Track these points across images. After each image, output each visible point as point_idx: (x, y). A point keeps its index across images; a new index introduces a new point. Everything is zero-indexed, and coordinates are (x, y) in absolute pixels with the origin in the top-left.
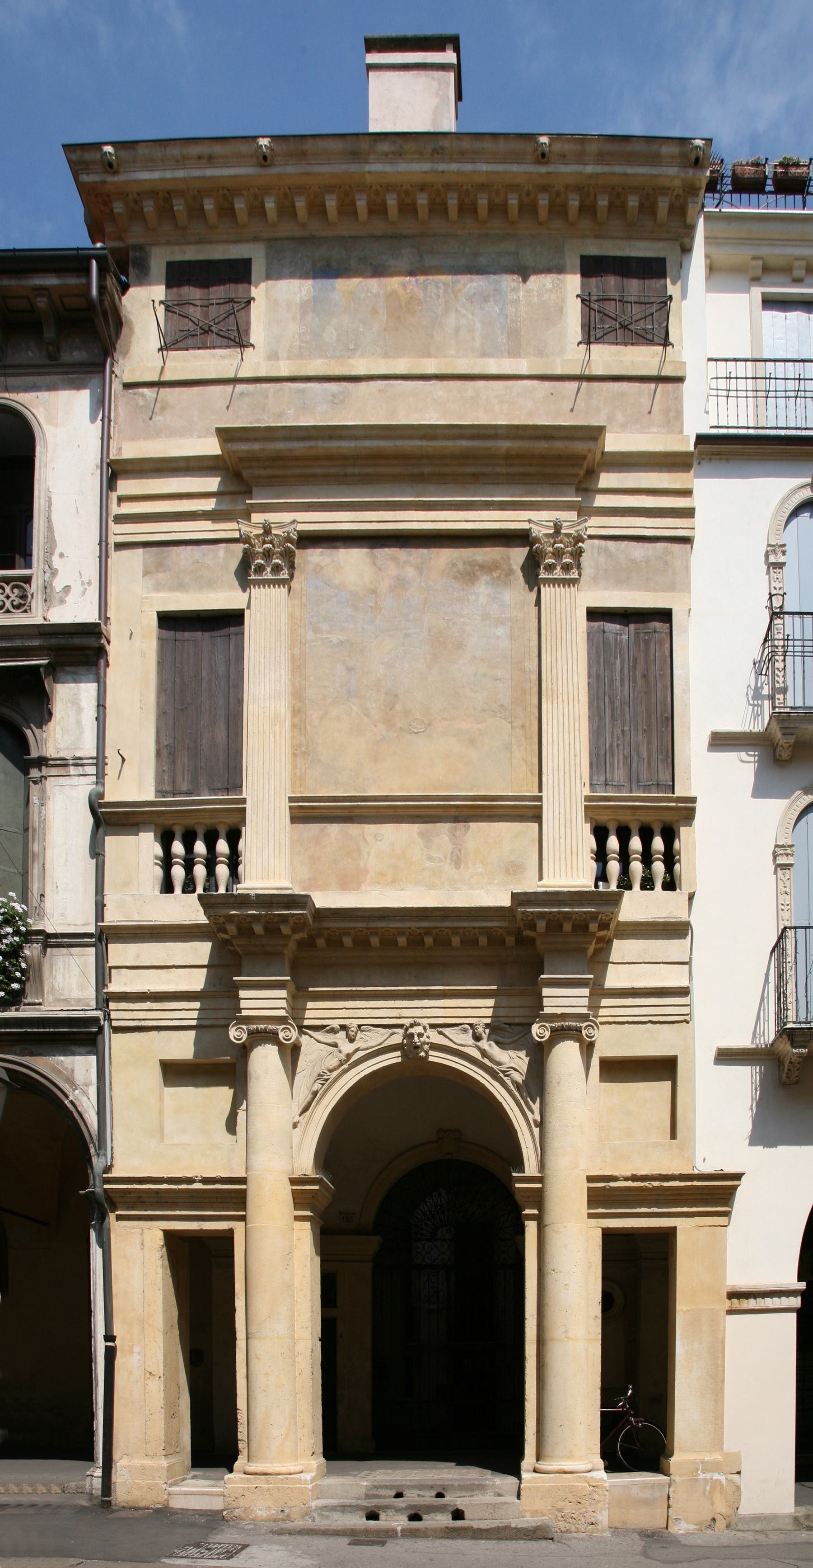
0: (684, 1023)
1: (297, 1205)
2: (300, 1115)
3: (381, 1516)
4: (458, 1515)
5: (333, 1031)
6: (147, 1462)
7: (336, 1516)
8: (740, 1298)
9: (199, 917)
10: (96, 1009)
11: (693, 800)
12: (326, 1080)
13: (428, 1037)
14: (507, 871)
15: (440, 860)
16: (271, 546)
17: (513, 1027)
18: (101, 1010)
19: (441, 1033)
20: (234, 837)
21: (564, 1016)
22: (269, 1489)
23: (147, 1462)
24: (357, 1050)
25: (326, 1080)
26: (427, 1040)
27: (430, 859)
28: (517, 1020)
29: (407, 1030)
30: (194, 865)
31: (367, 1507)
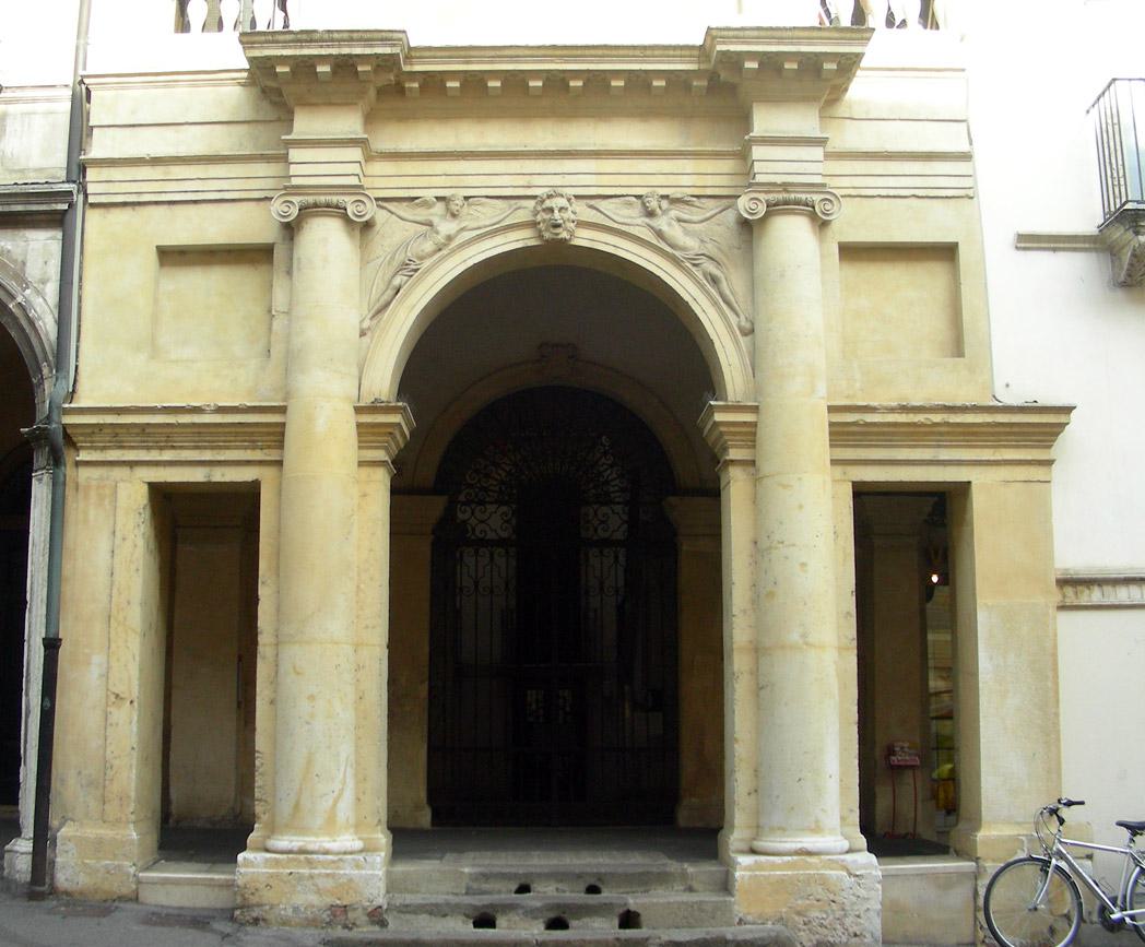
0: (966, 200)
1: (363, 443)
2: (372, 318)
3: (497, 922)
4: (629, 919)
5: (426, 204)
6: (106, 832)
7: (423, 919)
10: (68, 182)
12: (416, 270)
13: (574, 213)
18: (74, 182)
21: (785, 187)
22: (311, 877)
23: (106, 832)
24: (463, 229)
25: (416, 270)
26: (573, 217)
28: (709, 192)
29: (543, 202)
31: (475, 908)
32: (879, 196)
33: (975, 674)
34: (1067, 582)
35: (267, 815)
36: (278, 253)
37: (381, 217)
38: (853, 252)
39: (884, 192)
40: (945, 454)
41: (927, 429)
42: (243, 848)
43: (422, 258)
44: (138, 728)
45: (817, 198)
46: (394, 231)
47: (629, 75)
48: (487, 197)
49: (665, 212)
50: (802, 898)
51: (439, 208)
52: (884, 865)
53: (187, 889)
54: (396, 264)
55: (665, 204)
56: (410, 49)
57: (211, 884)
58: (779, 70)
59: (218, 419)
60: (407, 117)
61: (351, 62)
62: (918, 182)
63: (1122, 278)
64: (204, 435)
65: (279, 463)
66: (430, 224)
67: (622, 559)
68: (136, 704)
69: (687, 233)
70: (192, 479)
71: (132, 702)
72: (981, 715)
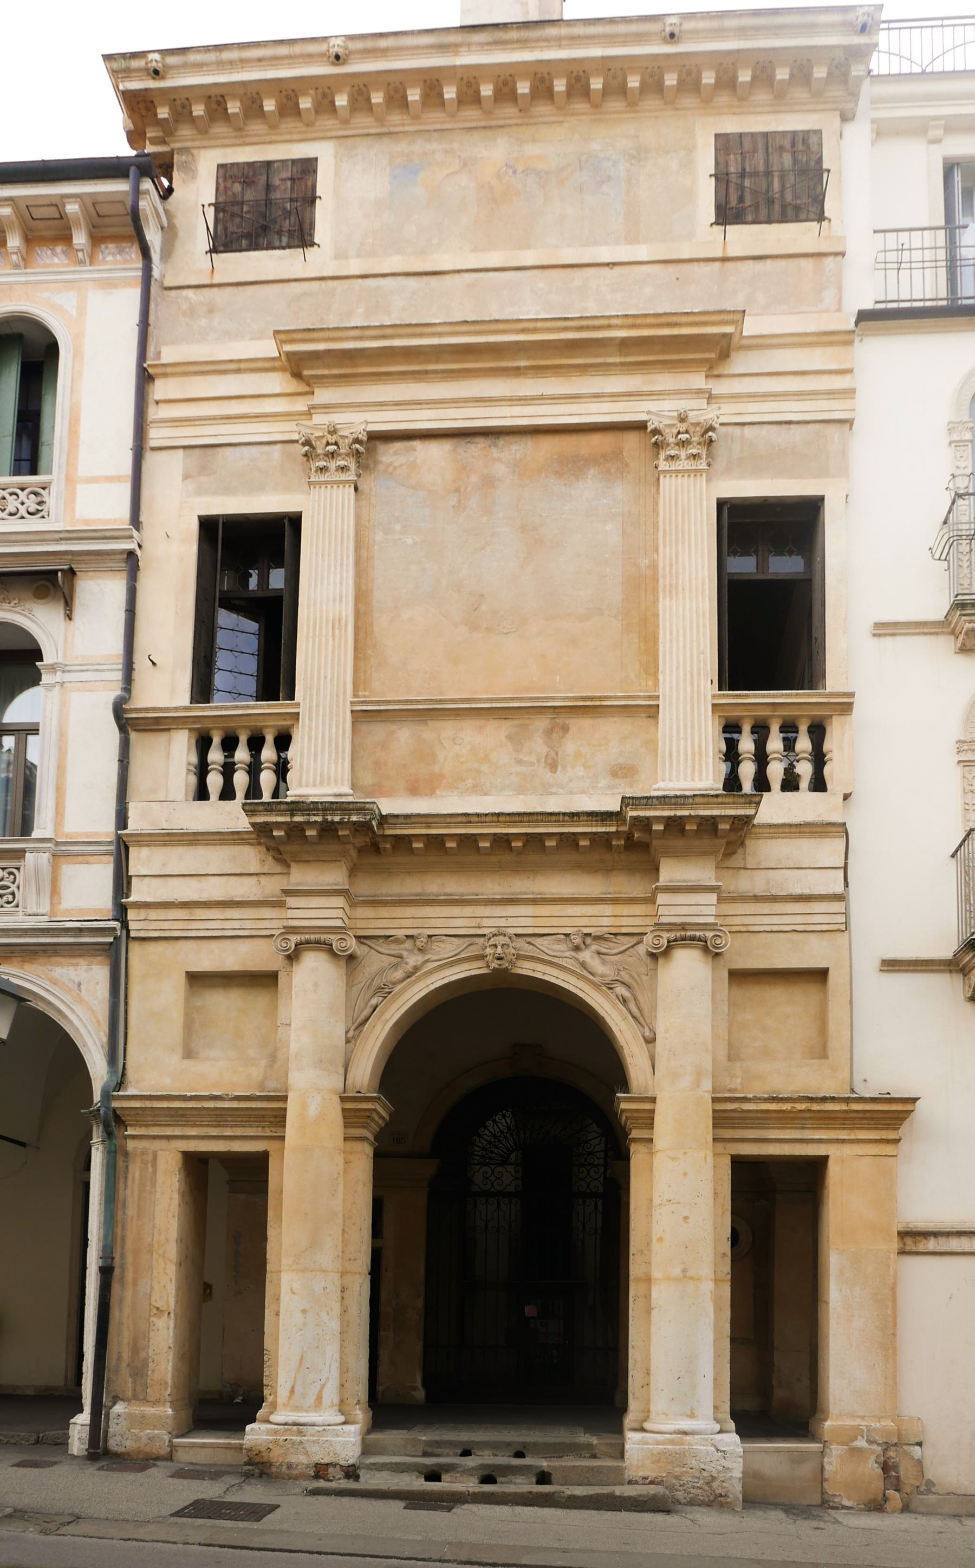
2: (355, 1030)
5: (398, 941)
9: (243, 823)
11: (852, 695)
16: (335, 447)
17: (619, 937)
19: (529, 943)
20: (283, 742)
21: (683, 927)
22: (301, 1442)
24: (427, 961)
25: (390, 993)
27: (519, 762)
28: (624, 930)
30: (234, 771)
32: (765, 931)
37: (360, 951)
38: (739, 977)
40: (808, 1134)
41: (794, 1115)
42: (253, 1420)
43: (395, 984)
44: (174, 1333)
45: (710, 934)
46: (375, 962)
48: (446, 935)
50: (678, 1466)
53: (210, 1450)
54: (373, 988)
56: (382, 817)
57: (228, 1447)
58: (682, 831)
59: (235, 1105)
60: (387, 872)
61: (333, 827)
62: (799, 919)
64: (220, 1117)
66: (401, 957)
67: (600, 1207)
68: (172, 1315)
69: (604, 962)
72: (831, 1333)
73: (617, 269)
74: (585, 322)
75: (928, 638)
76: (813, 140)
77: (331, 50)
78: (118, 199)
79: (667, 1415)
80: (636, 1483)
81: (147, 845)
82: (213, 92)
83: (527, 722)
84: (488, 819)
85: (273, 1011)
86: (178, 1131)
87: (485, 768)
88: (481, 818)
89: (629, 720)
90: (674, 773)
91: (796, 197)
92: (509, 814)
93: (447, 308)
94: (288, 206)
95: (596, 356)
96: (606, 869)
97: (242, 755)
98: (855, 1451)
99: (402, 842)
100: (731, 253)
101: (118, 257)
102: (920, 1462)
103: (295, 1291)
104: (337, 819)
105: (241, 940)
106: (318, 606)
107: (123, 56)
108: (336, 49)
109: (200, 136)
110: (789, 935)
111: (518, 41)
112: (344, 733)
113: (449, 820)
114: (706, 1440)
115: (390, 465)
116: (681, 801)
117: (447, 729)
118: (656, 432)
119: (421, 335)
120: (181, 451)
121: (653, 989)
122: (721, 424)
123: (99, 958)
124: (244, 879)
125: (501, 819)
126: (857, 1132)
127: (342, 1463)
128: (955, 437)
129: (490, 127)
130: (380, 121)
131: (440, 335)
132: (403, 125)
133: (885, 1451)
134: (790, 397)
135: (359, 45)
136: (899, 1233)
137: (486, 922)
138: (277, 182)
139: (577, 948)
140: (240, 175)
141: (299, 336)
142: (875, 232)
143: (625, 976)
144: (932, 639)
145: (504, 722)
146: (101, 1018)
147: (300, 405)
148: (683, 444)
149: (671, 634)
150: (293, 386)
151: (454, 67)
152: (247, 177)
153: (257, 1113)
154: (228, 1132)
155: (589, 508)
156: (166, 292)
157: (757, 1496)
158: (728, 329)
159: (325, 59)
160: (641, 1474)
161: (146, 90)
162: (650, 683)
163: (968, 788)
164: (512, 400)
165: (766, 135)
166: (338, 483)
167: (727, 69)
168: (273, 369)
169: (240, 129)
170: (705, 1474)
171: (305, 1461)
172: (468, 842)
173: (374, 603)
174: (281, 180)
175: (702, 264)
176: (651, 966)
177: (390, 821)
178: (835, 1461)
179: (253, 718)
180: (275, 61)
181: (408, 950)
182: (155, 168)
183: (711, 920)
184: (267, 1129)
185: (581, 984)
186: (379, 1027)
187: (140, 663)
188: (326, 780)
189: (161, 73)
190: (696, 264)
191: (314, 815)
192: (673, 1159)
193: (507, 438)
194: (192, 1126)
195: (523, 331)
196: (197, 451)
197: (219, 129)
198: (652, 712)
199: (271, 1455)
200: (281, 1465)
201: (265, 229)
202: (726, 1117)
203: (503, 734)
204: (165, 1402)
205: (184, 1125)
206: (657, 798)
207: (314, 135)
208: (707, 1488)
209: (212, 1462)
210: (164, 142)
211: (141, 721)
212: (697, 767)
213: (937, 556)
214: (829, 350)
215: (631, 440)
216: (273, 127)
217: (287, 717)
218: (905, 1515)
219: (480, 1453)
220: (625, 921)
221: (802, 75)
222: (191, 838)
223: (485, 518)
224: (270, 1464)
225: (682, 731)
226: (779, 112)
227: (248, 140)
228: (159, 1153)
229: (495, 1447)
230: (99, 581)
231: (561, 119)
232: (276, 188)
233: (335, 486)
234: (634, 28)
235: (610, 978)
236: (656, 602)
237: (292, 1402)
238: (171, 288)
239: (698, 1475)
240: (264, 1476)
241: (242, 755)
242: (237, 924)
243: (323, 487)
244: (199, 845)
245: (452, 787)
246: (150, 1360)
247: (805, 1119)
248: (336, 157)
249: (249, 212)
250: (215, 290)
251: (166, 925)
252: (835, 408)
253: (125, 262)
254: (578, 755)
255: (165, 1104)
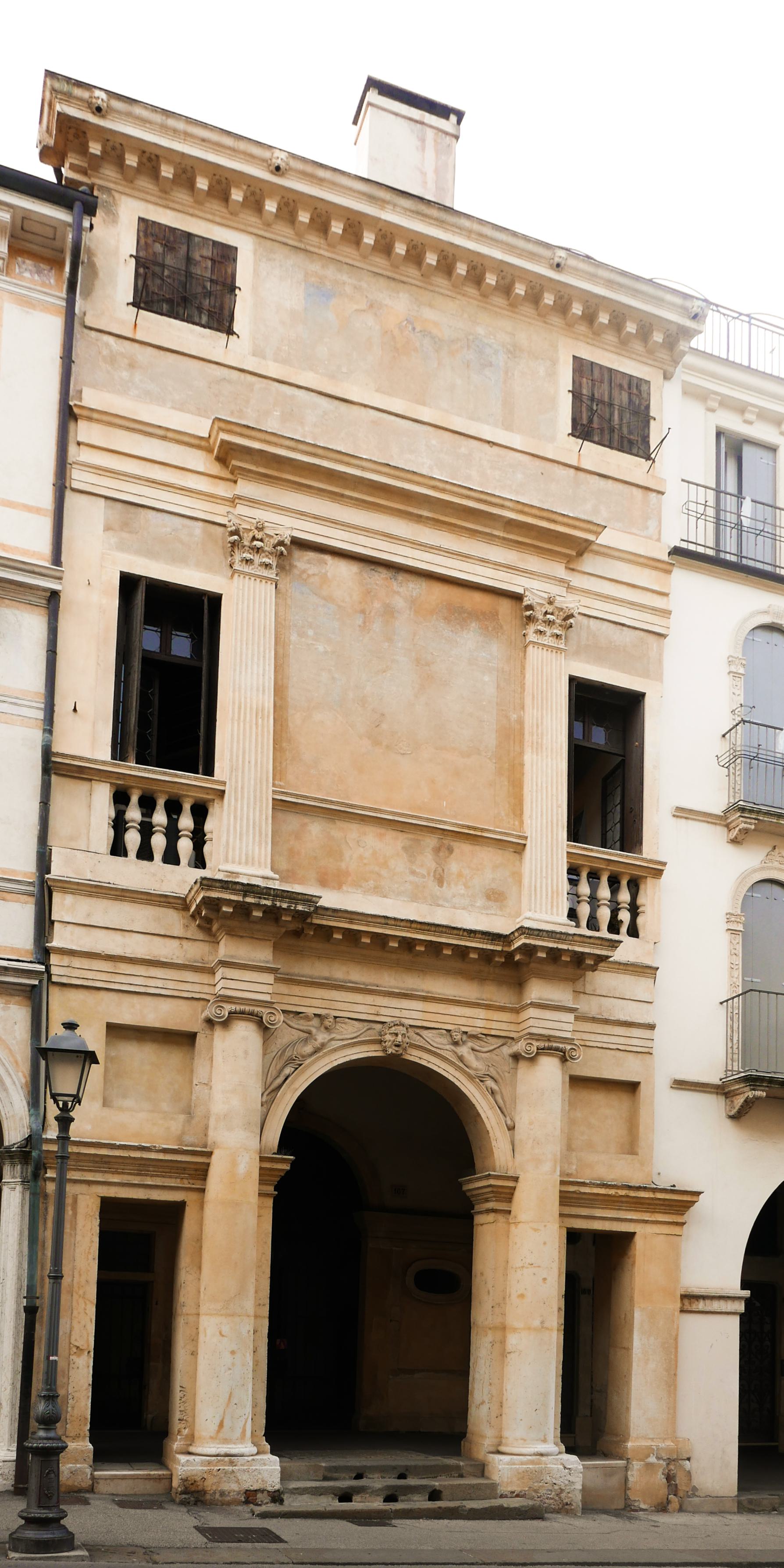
1: (262, 1182)
5: (307, 1018)
8: (691, 1301)
11: (664, 864)
14: (488, 897)
15: (423, 876)
19: (417, 1034)
21: (549, 1038)
22: (233, 1471)
25: (300, 1065)
27: (413, 873)
33: (628, 1349)
34: (689, 1298)
35: (187, 1430)
36: (200, 1040)
38: (577, 1082)
39: (599, 1045)
47: (375, 936)
49: (464, 1043)
51: (316, 1022)
52: (585, 1460)
53: (130, 1482)
54: (285, 1058)
55: (465, 1038)
57: (148, 1478)
60: (300, 954)
62: (622, 1040)
63: (732, 1113)
64: (143, 1167)
65: (203, 1191)
66: (309, 1033)
69: (477, 1058)
70: (135, 1197)
71: (89, 1352)
73: (495, 448)
74: (484, 497)
75: (710, 825)
76: (644, 388)
77: (274, 160)
78: (52, 224)
79: (525, 1440)
80: (506, 1496)
81: (72, 893)
82: (148, 149)
83: (420, 838)
84: (402, 924)
85: (189, 1070)
86: (99, 1177)
87: (384, 872)
88: (397, 922)
89: (500, 852)
90: (538, 906)
91: (630, 433)
92: (421, 923)
93: (361, 441)
94: (208, 285)
95: (485, 526)
96: (480, 978)
97: (160, 818)
98: (649, 1466)
99: (326, 932)
100: (584, 465)
101: (36, 277)
102: (689, 1473)
103: (223, 1333)
104: (285, 906)
105: (162, 999)
106: (243, 692)
107: (68, 80)
108: (279, 161)
109: (124, 183)
110: (612, 1052)
111: (436, 219)
112: (267, 819)
113: (370, 919)
114: (557, 1460)
115: (304, 571)
116: (563, 937)
117: (353, 830)
118: (530, 607)
119: (348, 464)
120: (103, 500)
121: (514, 1084)
122: (579, 613)
123: (17, 998)
124: (167, 940)
125: (414, 925)
126: (656, 1215)
127: (270, 1489)
128: (733, 669)
129: (394, 279)
130: (300, 236)
131: (363, 469)
132: (320, 248)
133: (668, 1464)
134: (625, 604)
135: (300, 166)
136: (681, 1296)
137: (383, 1011)
138: (197, 257)
139: (456, 1044)
140: (161, 236)
141: (238, 429)
142: (683, 480)
143: (493, 1073)
144: (712, 827)
145: (400, 834)
146: (19, 1058)
147: (223, 490)
148: (550, 623)
149: (537, 785)
150: (215, 469)
151: (379, 219)
152: (168, 241)
153: (179, 1165)
154: (149, 1181)
155: (470, 655)
156: (86, 331)
157: (592, 1505)
158: (591, 537)
159: (265, 164)
160: (510, 1489)
161: (84, 121)
162: (517, 823)
163: (733, 951)
164: (414, 544)
165: (610, 370)
166: (262, 578)
167: (592, 308)
168: (199, 447)
169: (166, 192)
170: (556, 1487)
171: (237, 1489)
172: (381, 940)
173: (289, 700)
174: (202, 256)
175: (561, 467)
176: (512, 1066)
177: (320, 912)
178: (634, 1476)
179: (177, 786)
180: (218, 147)
181: (316, 1028)
182: (79, 200)
183: (568, 1035)
184: (186, 1181)
185: (458, 1074)
186: (288, 1096)
187: (62, 706)
188: (250, 859)
189: (103, 112)
190: (556, 465)
191: (265, 899)
192: (536, 1230)
193: (407, 576)
194: (113, 1173)
195: (434, 488)
196: (119, 506)
197: (144, 183)
198: (520, 848)
199: (206, 1483)
200: (215, 1493)
201: (185, 300)
202: (570, 1197)
203: (399, 844)
204: (85, 1436)
205: (105, 1172)
206: (547, 931)
207: (235, 225)
208: (557, 1498)
209: (132, 1492)
210: (84, 173)
211: (64, 767)
212: (555, 904)
213: (722, 764)
214: (654, 573)
215: (505, 606)
216: (199, 203)
217: (210, 792)
218: (681, 1514)
219: (371, 1476)
220: (495, 1025)
221: (644, 333)
222: (118, 893)
223: (387, 644)
224: (204, 1492)
225: (544, 870)
226: (619, 354)
227: (172, 205)
228: (80, 1197)
229: (383, 1470)
230: (17, 612)
231: (454, 295)
232: (197, 263)
233: (258, 580)
234: (530, 247)
235: (483, 1072)
236: (521, 753)
237: (221, 1435)
238: (91, 329)
239: (550, 1488)
240: (199, 1503)
241: (160, 818)
242: (160, 983)
243: (247, 577)
244: (125, 901)
245: (356, 885)
246: (70, 1397)
247: (622, 1202)
248: (255, 254)
249: (169, 277)
250: (136, 345)
251: (90, 975)
252: (654, 623)
253: (43, 284)
254: (460, 875)
255: (92, 1151)
